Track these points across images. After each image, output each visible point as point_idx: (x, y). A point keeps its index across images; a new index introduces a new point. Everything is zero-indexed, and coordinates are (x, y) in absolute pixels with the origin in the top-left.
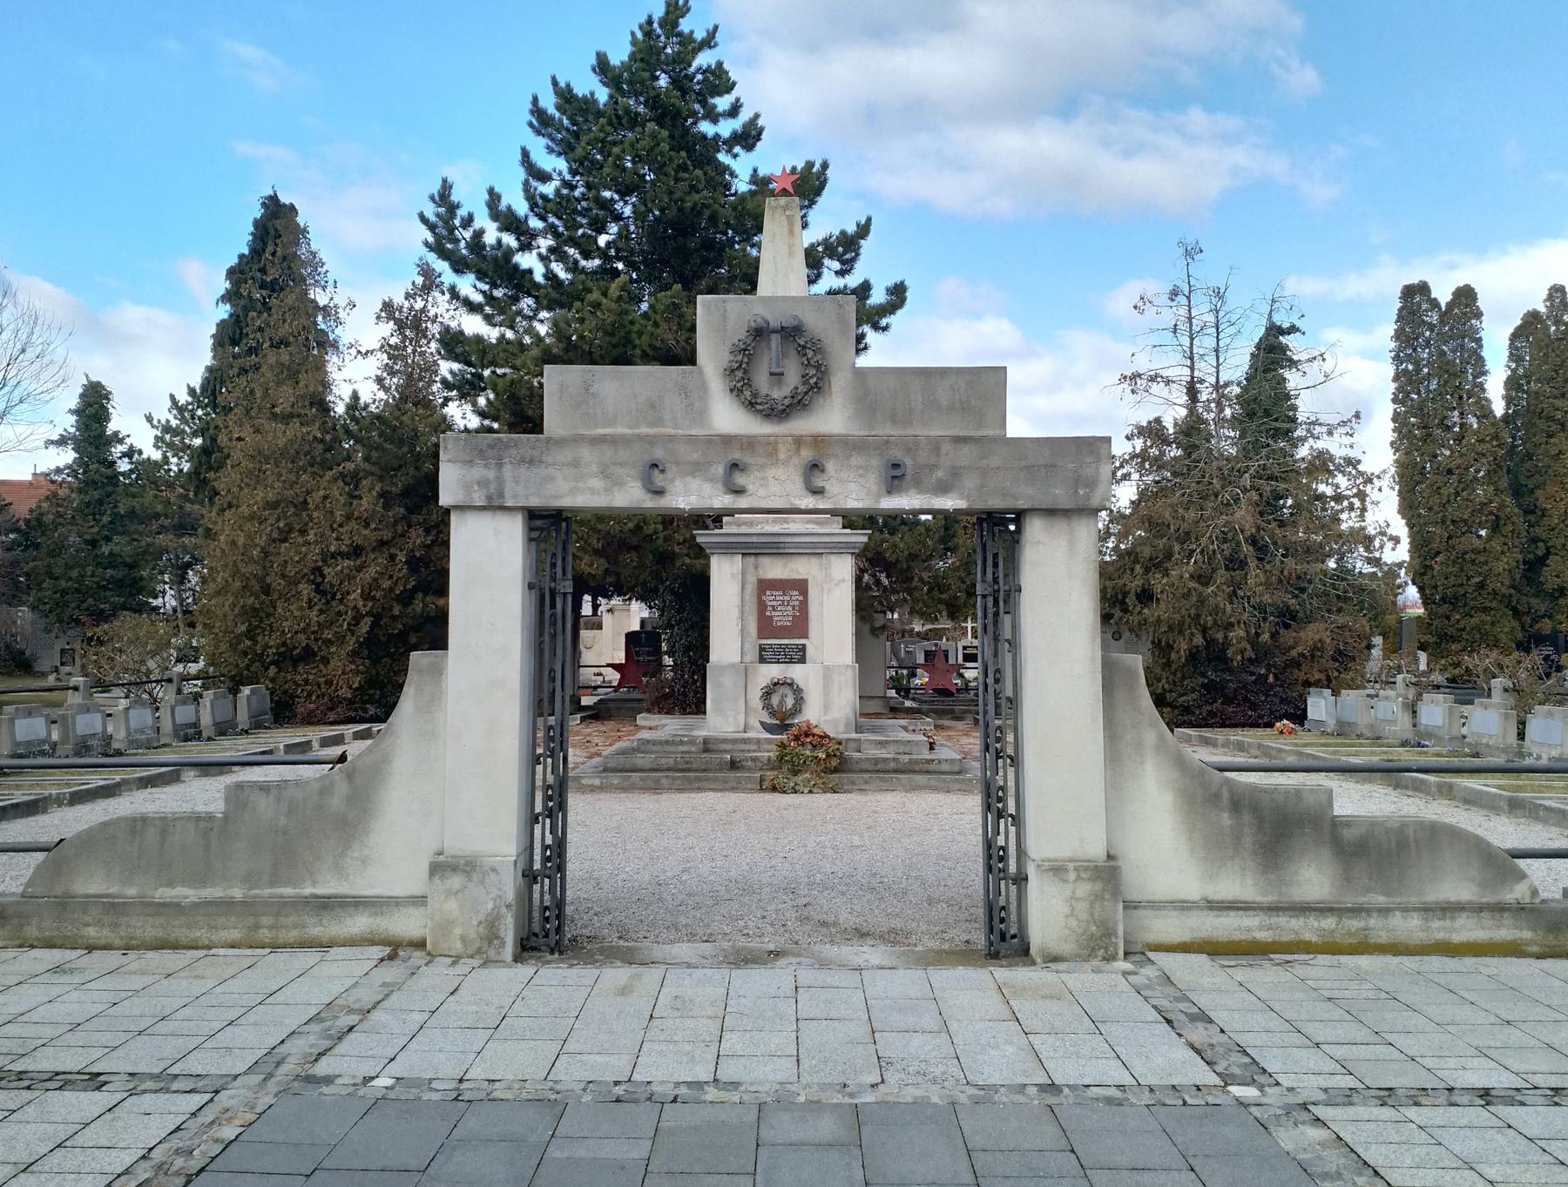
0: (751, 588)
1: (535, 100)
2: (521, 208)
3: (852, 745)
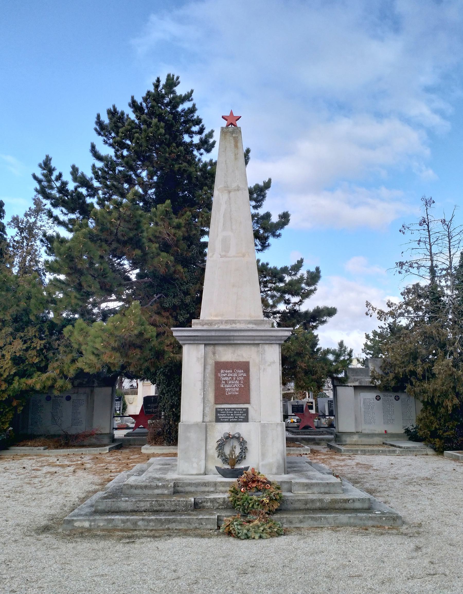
0: (210, 368)
1: (98, 116)
2: (89, 174)
3: (285, 486)
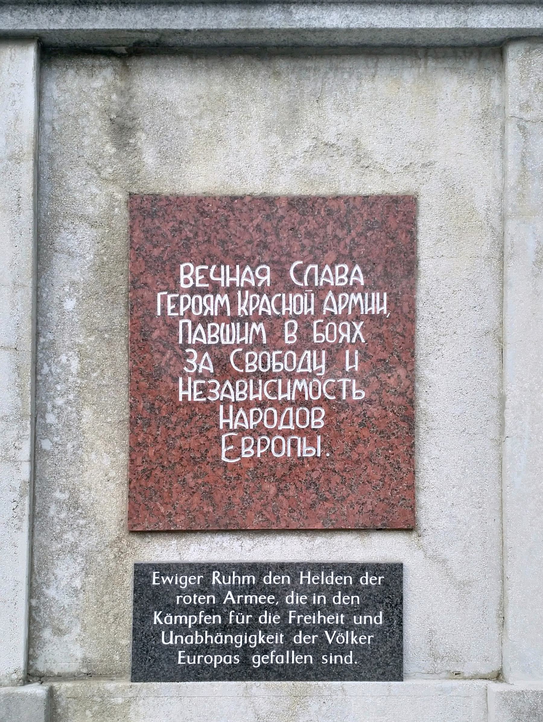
0: (88, 250)
